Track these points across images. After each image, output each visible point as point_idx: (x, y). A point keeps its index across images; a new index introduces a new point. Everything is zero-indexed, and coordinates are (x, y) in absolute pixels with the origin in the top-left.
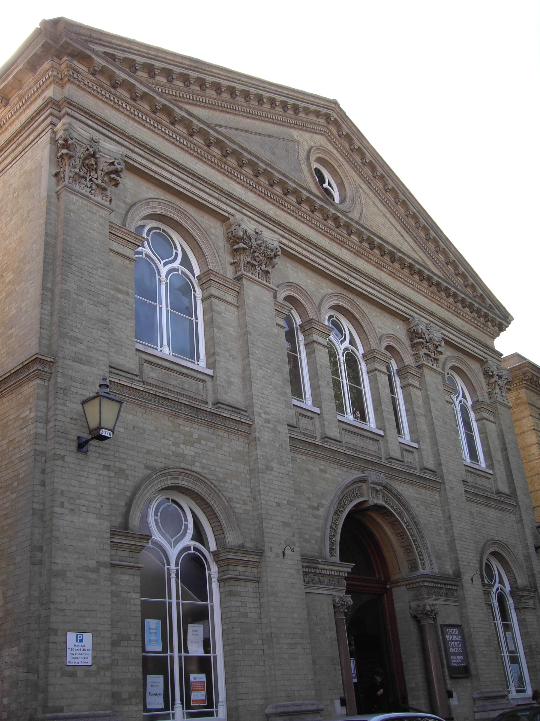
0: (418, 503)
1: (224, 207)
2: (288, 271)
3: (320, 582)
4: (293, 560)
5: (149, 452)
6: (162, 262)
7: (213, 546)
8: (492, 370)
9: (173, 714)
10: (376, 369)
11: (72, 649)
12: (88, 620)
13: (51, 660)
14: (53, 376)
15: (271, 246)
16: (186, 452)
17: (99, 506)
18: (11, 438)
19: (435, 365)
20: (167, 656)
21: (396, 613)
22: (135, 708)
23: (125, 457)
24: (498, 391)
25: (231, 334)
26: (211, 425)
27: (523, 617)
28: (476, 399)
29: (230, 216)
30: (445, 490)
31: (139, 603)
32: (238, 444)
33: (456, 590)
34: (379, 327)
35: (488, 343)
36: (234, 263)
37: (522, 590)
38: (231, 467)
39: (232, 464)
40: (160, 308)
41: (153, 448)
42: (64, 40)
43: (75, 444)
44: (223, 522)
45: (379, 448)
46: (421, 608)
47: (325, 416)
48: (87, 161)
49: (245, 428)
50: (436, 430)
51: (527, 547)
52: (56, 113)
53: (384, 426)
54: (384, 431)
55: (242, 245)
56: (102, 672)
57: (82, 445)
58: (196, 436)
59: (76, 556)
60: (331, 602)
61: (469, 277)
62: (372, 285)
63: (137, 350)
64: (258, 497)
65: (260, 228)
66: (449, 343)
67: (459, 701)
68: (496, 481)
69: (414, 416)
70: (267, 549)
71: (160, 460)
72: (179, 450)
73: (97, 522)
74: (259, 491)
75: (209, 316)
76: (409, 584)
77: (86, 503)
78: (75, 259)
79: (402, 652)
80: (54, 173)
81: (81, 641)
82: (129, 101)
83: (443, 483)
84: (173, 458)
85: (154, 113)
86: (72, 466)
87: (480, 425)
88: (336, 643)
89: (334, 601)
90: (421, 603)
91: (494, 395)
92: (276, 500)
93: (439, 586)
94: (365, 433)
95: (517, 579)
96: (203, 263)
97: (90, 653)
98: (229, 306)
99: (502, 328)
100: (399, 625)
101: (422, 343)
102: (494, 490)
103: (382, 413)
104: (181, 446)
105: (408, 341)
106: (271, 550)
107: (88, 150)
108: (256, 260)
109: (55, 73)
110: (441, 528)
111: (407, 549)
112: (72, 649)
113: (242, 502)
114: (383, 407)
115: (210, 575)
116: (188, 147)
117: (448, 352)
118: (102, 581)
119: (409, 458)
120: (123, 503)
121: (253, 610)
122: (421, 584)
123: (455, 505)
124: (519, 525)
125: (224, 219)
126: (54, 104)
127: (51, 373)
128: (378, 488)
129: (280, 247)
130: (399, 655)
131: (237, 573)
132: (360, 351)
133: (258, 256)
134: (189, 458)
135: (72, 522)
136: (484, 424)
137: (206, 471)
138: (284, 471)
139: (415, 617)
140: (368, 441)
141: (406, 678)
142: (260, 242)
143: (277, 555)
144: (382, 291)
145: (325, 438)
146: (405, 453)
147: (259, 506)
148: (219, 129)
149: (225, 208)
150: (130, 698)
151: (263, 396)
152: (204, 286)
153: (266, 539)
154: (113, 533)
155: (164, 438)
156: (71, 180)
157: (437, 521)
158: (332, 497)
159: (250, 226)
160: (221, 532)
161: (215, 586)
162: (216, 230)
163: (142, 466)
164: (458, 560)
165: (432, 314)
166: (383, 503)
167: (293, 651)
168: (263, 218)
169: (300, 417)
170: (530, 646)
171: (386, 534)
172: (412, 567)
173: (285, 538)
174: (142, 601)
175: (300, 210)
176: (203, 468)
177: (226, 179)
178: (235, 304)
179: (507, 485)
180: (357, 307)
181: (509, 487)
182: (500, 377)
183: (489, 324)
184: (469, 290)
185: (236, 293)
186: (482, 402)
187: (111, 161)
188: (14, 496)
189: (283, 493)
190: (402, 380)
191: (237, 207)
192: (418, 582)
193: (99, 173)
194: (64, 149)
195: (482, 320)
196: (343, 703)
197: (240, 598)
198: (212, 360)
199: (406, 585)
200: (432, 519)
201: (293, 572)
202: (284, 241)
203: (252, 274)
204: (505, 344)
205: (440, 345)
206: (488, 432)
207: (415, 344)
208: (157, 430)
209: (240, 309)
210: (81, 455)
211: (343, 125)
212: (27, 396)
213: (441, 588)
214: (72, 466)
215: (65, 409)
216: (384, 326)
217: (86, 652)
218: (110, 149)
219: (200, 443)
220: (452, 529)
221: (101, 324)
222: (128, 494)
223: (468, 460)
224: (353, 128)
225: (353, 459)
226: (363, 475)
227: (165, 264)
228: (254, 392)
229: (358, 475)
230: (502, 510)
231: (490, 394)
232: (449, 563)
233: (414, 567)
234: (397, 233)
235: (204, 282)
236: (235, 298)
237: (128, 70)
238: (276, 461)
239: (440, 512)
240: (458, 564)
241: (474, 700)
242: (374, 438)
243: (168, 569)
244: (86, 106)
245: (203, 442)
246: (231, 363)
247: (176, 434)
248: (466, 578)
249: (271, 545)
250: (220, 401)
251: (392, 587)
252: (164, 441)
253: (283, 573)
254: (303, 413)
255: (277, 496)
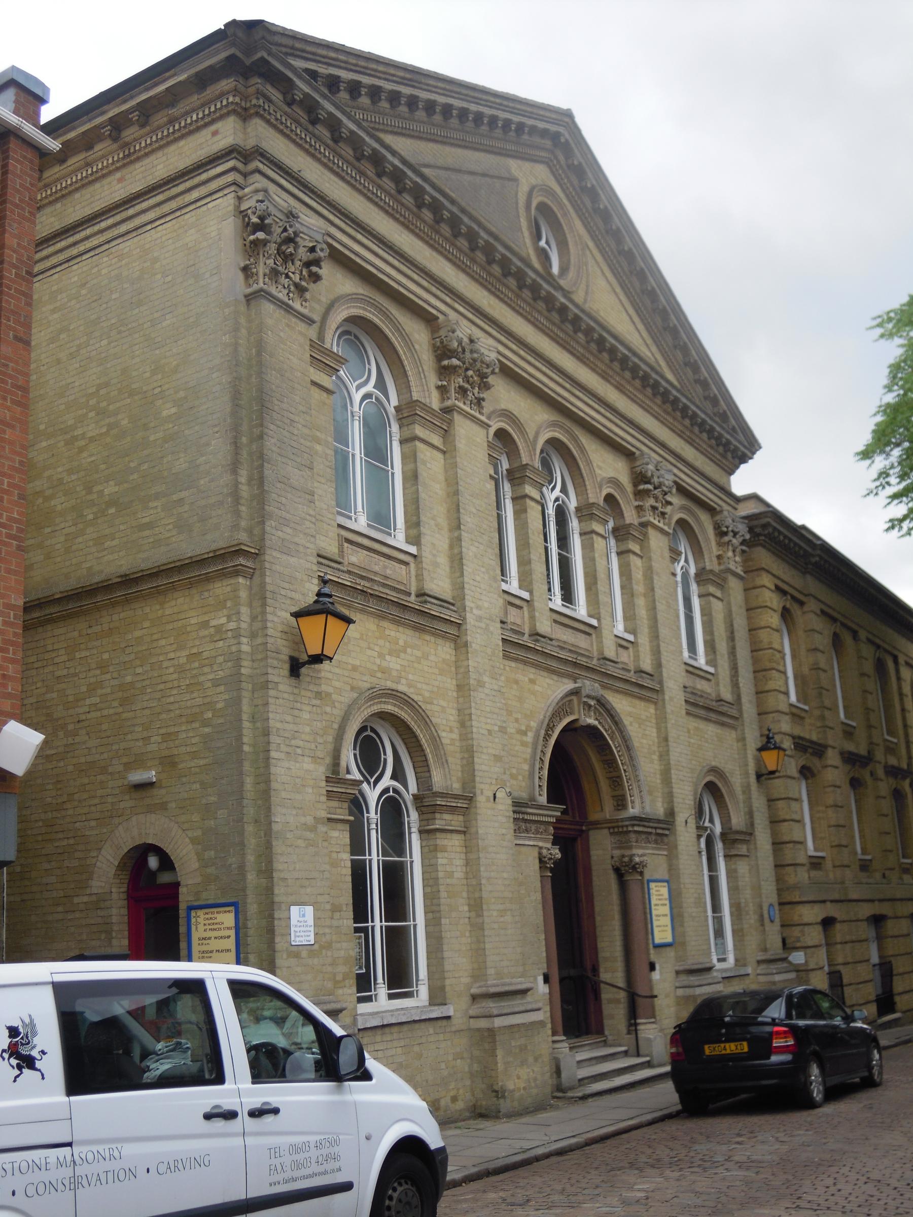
0: (631, 719)
1: (433, 300)
2: (504, 396)
3: (527, 831)
4: (504, 805)
5: (355, 668)
6: (355, 385)
7: (413, 787)
8: (727, 524)
9: (376, 995)
10: (593, 532)
11: (296, 926)
12: (309, 890)
13: (277, 939)
14: (257, 572)
15: (487, 359)
16: (392, 665)
17: (313, 746)
18: (195, 651)
19: (662, 521)
20: (368, 927)
21: (593, 863)
22: (349, 991)
23: (331, 677)
24: (730, 554)
25: (436, 493)
26: (418, 628)
27: (733, 867)
28: (701, 565)
29: (439, 315)
30: (664, 700)
31: (349, 864)
32: (444, 651)
33: (666, 835)
34: (598, 466)
35: (721, 481)
36: (442, 386)
37: (738, 832)
38: (437, 683)
39: (439, 678)
40: (353, 455)
41: (358, 663)
42: (259, 55)
43: (287, 666)
44: (430, 756)
45: (592, 644)
46: (626, 859)
47: (536, 604)
48: (284, 248)
49: (453, 631)
50: (659, 617)
51: (747, 774)
52: (240, 165)
53: (599, 613)
54: (599, 620)
55: (455, 362)
56: (324, 951)
57: (295, 668)
58: (401, 643)
59: (294, 812)
60: (537, 855)
61: (713, 386)
62: (596, 406)
63: (339, 526)
64: (468, 724)
65: (477, 333)
66: (682, 491)
67: (661, 974)
68: (717, 684)
69: (633, 596)
70: (478, 792)
71: (365, 678)
72: (384, 664)
73: (311, 767)
74: (470, 714)
75: (411, 466)
76: (613, 828)
77: (301, 743)
78: (276, 402)
79: (596, 912)
80: (242, 265)
81: (304, 916)
82: (330, 142)
83: (659, 691)
84: (379, 675)
85: (358, 160)
86: (286, 696)
87: (703, 603)
88: (540, 906)
89: (540, 854)
90: (627, 852)
91: (725, 560)
92: (489, 727)
93: (649, 830)
94: (576, 625)
95: (732, 817)
96: (403, 386)
97: (312, 929)
98: (435, 452)
99: (744, 459)
100: (595, 879)
101: (649, 491)
102: (714, 696)
103: (597, 595)
104: (388, 657)
105: (631, 485)
106: (482, 793)
107: (285, 230)
108: (468, 382)
109: (237, 99)
110: (654, 753)
111: (614, 781)
112: (296, 926)
113: (448, 729)
114: (599, 586)
115: (409, 823)
116: (393, 209)
117: (676, 500)
118: (320, 842)
119: (625, 657)
120: (330, 739)
121: (459, 869)
122: (630, 829)
123: (673, 721)
124: (740, 744)
125: (429, 320)
126: (239, 153)
127: (254, 569)
128: (592, 703)
129: (499, 360)
130: (592, 916)
131: (443, 822)
132: (572, 504)
133: (472, 377)
134: (394, 674)
135: (289, 769)
136: (709, 603)
137: (412, 690)
138: (496, 688)
139: (617, 870)
140: (580, 635)
141: (600, 945)
142: (475, 355)
143: (488, 800)
144: (522, 353)
145: (536, 635)
146: (621, 650)
147: (469, 736)
148: (426, 171)
149: (433, 302)
150: (344, 980)
151: (475, 583)
152: (404, 421)
153: (477, 779)
154: (328, 780)
155: (369, 648)
156: (267, 280)
157: (651, 743)
158: (542, 717)
159: (465, 330)
160: (426, 769)
161: (415, 837)
162: (419, 335)
163: (348, 688)
164: (672, 796)
165: (663, 445)
166: (596, 723)
167: (502, 919)
168: (489, 323)
169: (509, 607)
170: (739, 903)
171: (589, 760)
172: (618, 805)
173: (495, 776)
174: (352, 860)
175: (456, 246)
176: (410, 686)
177: (434, 254)
178: (442, 447)
179: (730, 689)
180: (575, 440)
181: (733, 693)
182: (735, 534)
183: (729, 455)
184: (708, 406)
185: (443, 432)
186: (711, 571)
187: (311, 245)
188: (207, 730)
189: (495, 716)
190: (620, 543)
191: (448, 300)
192: (627, 826)
193: (298, 263)
194: (255, 231)
195: (721, 449)
196: (546, 980)
197: (446, 855)
198: (413, 532)
199: (609, 828)
200: (645, 741)
201: (504, 820)
202: (333, 230)
203: (465, 403)
204: (743, 481)
205: (670, 492)
206: (714, 614)
207: (640, 491)
208: (361, 638)
209: (447, 455)
210: (293, 681)
211: (576, 151)
212: (221, 597)
213: (650, 833)
214: (286, 696)
215: (276, 619)
216: (606, 467)
217: (308, 929)
218: (312, 225)
219: (405, 652)
220: (668, 755)
221: (307, 496)
222: (336, 726)
223: (686, 654)
224: (589, 156)
225: (573, 665)
226: (577, 685)
227: (358, 388)
228: (466, 579)
229: (569, 685)
230: (723, 724)
231: (719, 557)
232: (660, 799)
233: (621, 803)
234: (628, 318)
235: (405, 415)
236: (441, 439)
237: (326, 92)
238: (487, 674)
239: (655, 730)
240: (672, 802)
241: (678, 973)
242: (587, 630)
243: (368, 817)
244: (565, 367)
245: (409, 650)
246: (437, 535)
247: (381, 642)
248: (680, 819)
249: (482, 786)
250: (427, 592)
251: (589, 830)
252: (369, 652)
253: (494, 820)
254: (512, 601)
255: (489, 721)
